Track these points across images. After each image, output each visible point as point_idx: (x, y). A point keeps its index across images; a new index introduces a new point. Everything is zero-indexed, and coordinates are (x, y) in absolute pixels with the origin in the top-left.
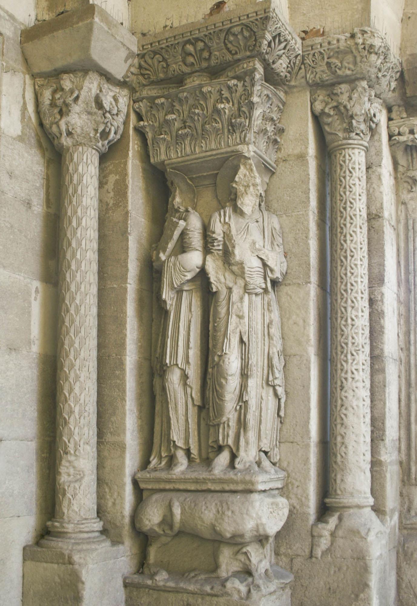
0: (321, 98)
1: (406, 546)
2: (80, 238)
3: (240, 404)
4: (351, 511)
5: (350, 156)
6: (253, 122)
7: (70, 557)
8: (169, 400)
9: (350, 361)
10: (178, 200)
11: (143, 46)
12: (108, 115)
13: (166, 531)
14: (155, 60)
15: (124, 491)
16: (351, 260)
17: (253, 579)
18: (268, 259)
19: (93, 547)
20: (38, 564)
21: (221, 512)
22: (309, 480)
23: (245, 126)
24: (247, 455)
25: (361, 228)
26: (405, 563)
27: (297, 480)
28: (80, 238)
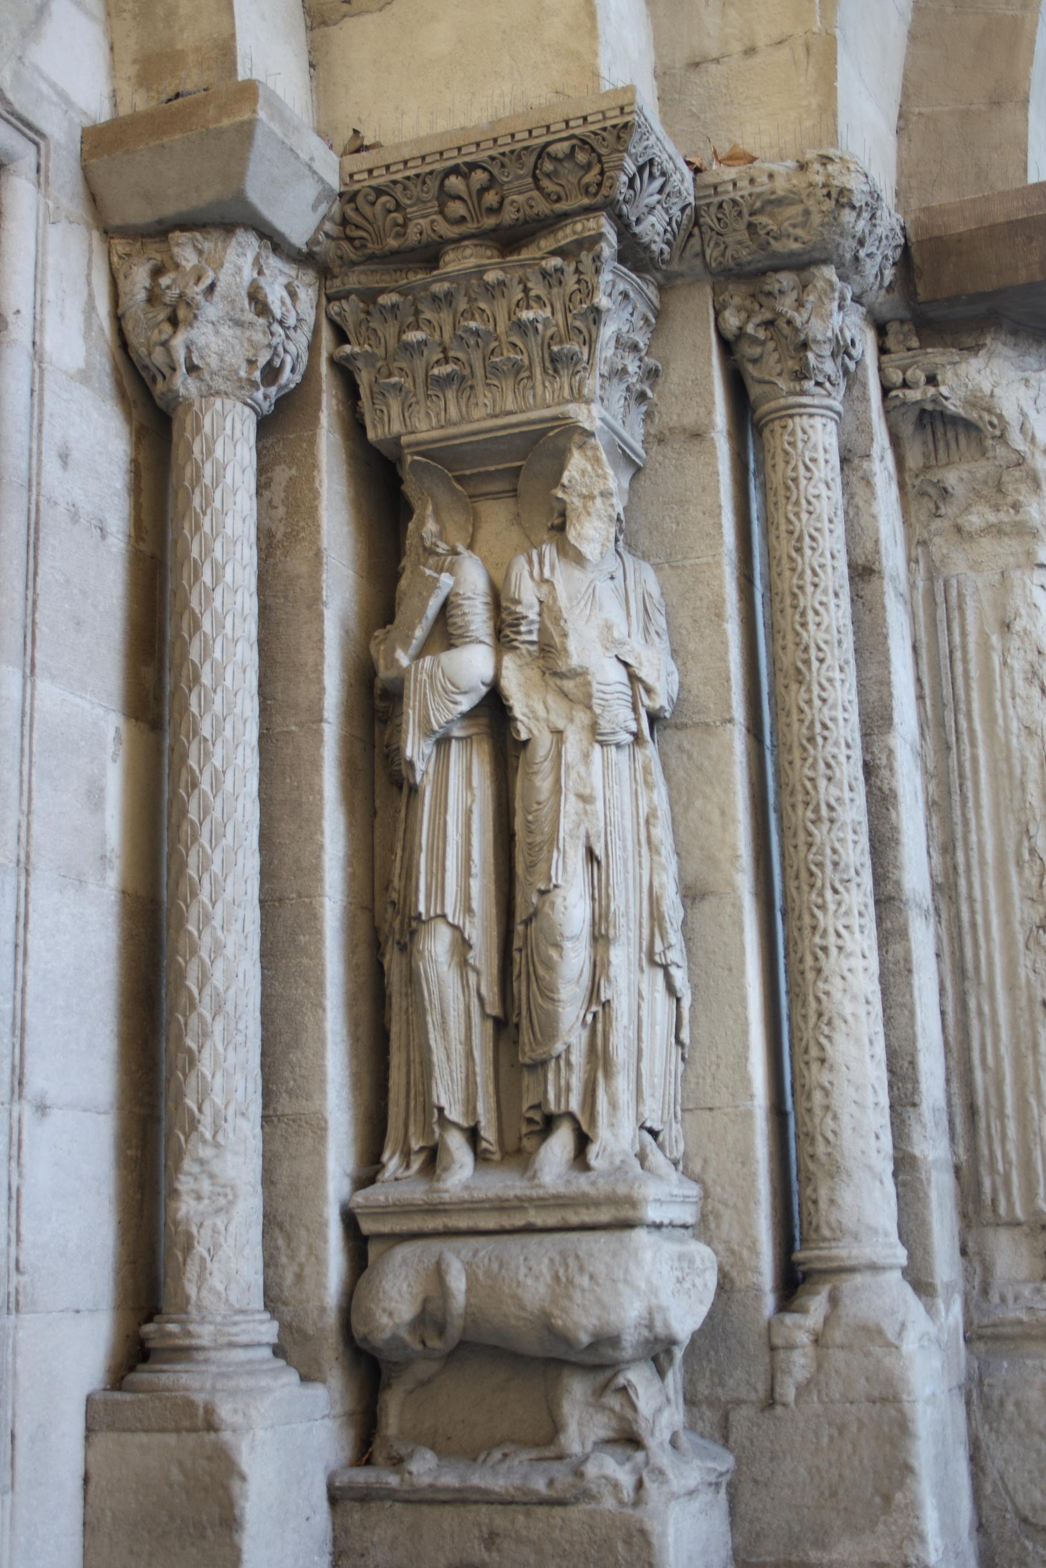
0: (737, 300)
1: (986, 1382)
2: (220, 610)
3: (594, 1008)
4: (858, 1279)
5: (804, 432)
6: (598, 353)
7: (209, 1411)
8: (427, 1004)
9: (832, 907)
10: (431, 526)
11: (351, 176)
12: (276, 328)
13: (429, 1343)
14: (378, 207)
15: (325, 1241)
16: (819, 669)
17: (647, 1456)
18: (640, 664)
19: (263, 1383)
20: (127, 1437)
21: (564, 1279)
22: (757, 1203)
23: (579, 360)
24: (615, 1135)
25: (836, 595)
26: (987, 1427)
27: (726, 1205)
28: (220, 610)
